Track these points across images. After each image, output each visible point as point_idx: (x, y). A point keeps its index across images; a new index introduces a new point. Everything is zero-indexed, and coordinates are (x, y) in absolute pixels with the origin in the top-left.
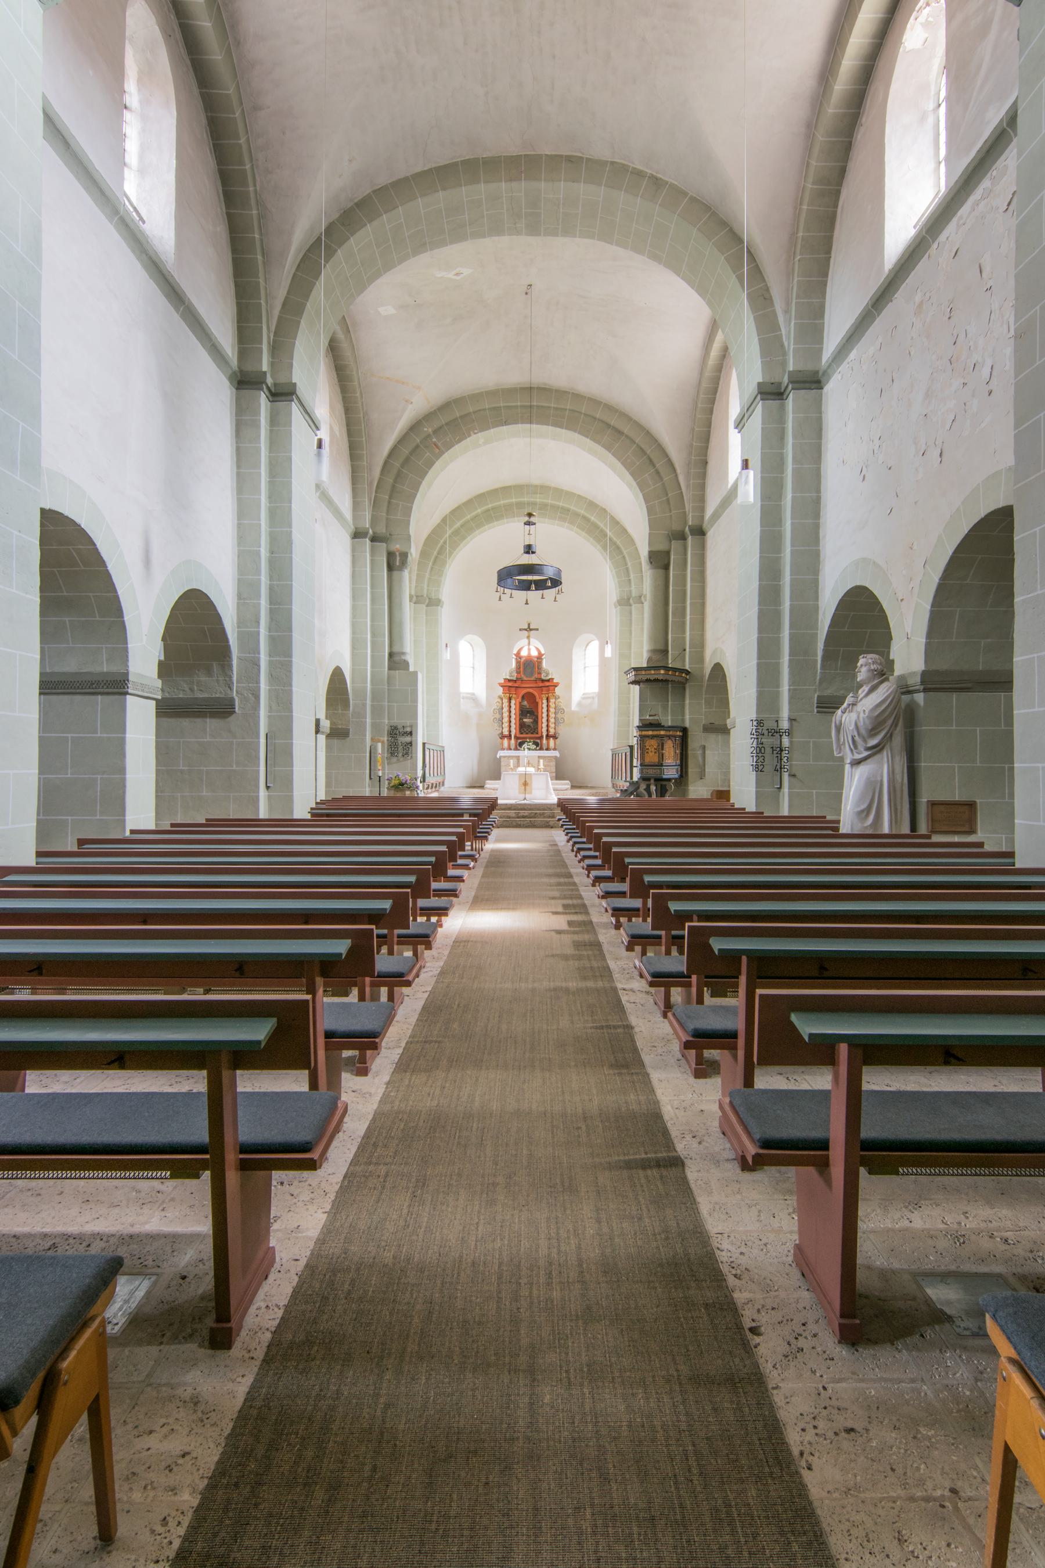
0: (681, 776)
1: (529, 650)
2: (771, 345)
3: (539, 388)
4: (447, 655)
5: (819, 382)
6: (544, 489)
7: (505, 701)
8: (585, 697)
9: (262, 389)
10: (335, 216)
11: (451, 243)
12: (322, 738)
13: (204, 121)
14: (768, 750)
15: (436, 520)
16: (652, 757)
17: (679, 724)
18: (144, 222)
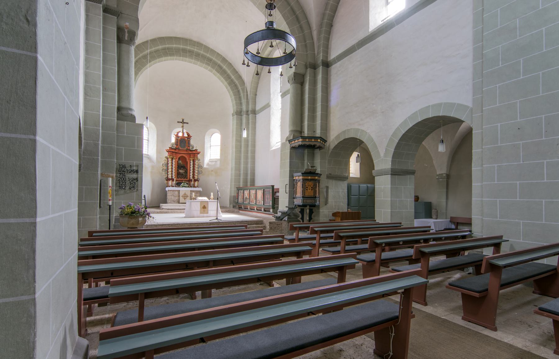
1: (183, 133)
7: (170, 160)
8: (211, 161)
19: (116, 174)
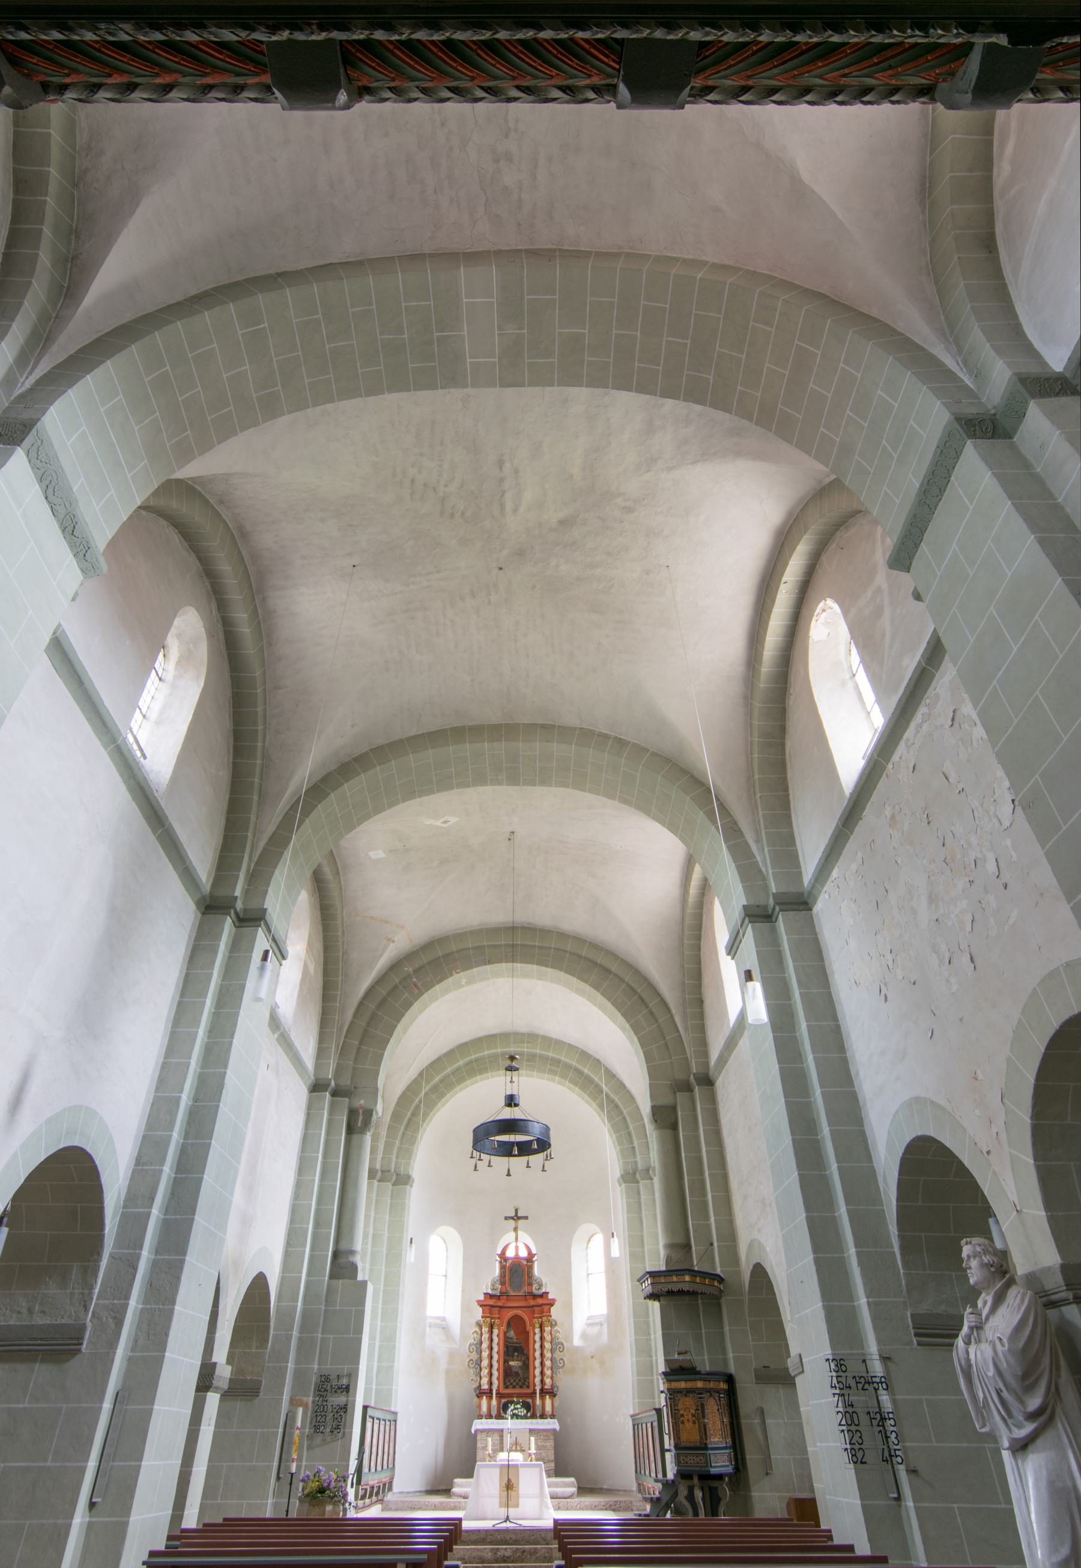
0: (737, 1469)
1: (517, 1248)
2: (749, 871)
3: (523, 928)
4: (410, 1256)
5: (806, 903)
6: (531, 1037)
7: (485, 1329)
9: (229, 914)
10: (333, 767)
11: (438, 791)
12: (213, 1400)
13: (229, 694)
14: (864, 1419)
15: (412, 1073)
16: (690, 1434)
17: (719, 1369)
18: (145, 758)
19: (314, 1397)
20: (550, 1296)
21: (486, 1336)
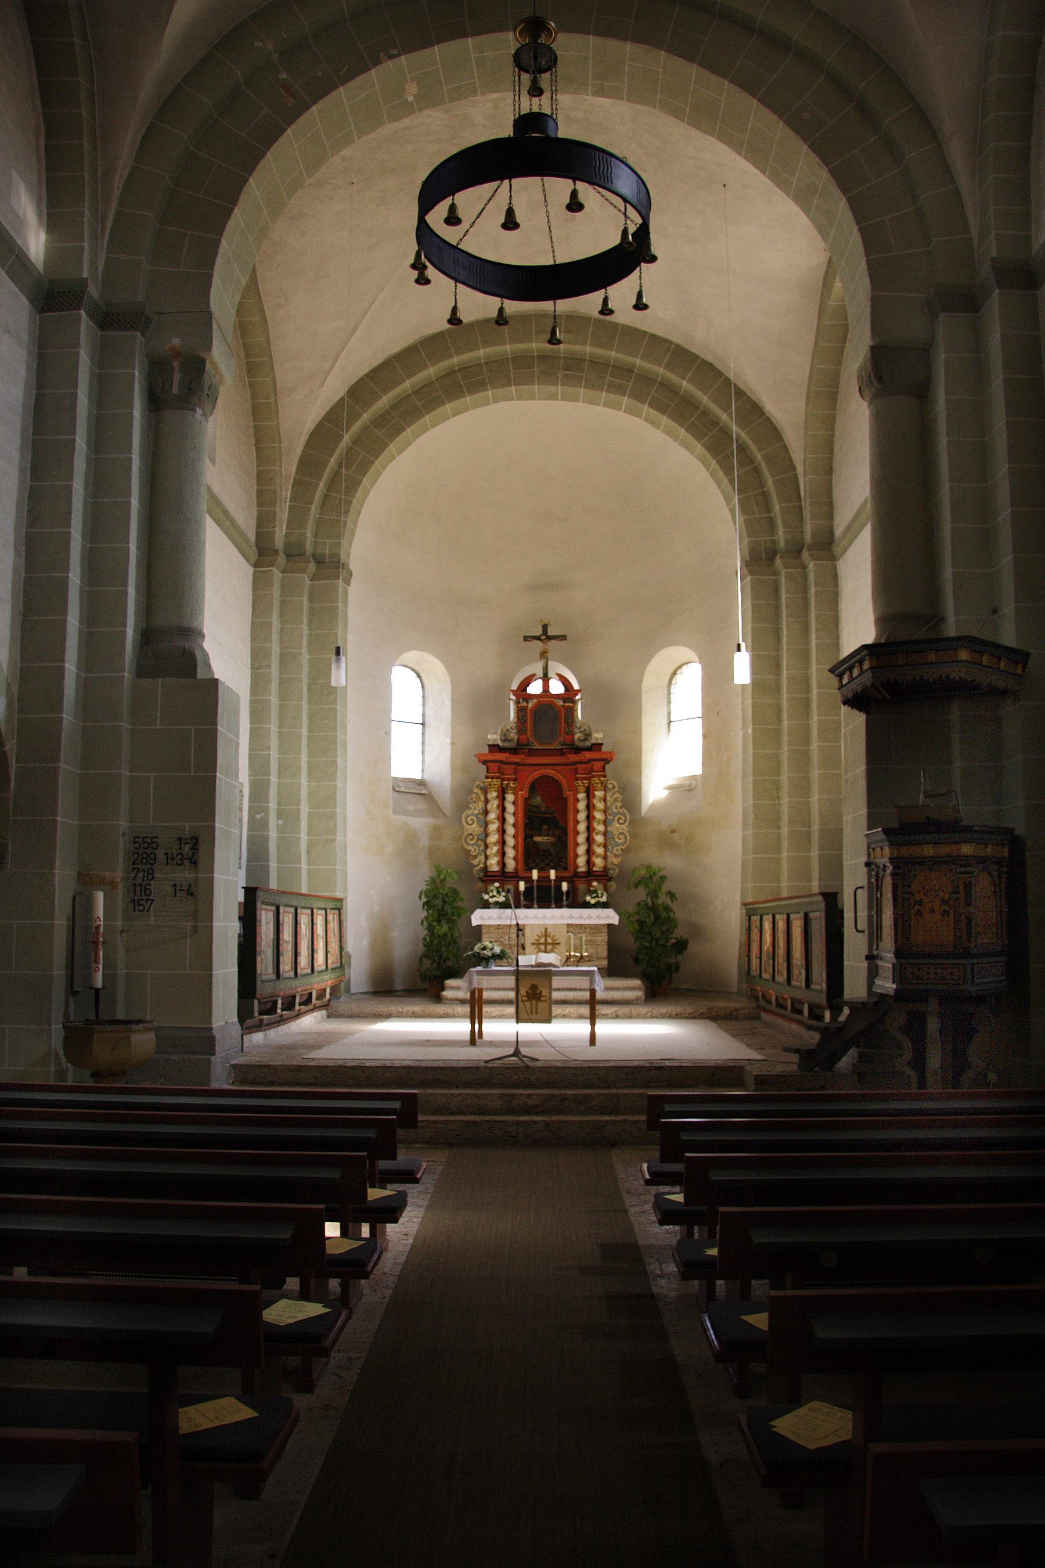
1: (546, 679)
7: (493, 794)
15: (333, 388)
20: (604, 749)
21: (494, 804)
